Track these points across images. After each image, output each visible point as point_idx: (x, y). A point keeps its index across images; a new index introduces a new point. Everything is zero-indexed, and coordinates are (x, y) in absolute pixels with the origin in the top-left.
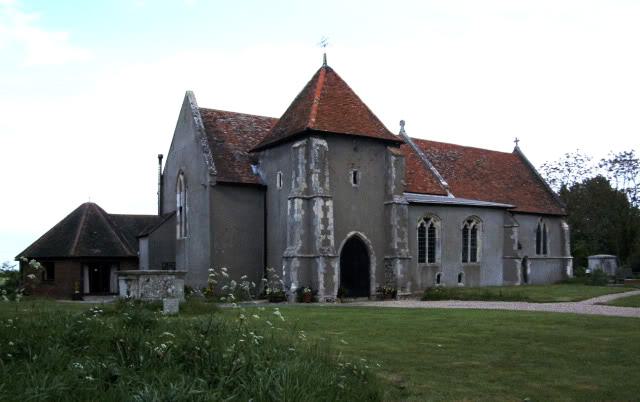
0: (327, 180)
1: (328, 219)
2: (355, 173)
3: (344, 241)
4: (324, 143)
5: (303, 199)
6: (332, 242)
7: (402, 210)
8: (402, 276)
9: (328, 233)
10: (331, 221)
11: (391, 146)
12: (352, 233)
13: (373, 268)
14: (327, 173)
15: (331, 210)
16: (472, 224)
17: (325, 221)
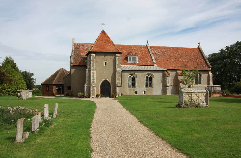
0: (95, 65)
1: (94, 76)
2: (106, 63)
3: (101, 82)
4: (94, 55)
5: (88, 70)
6: (95, 82)
7: (120, 72)
8: (118, 91)
9: (94, 79)
10: (95, 76)
11: (92, 53)
12: (104, 79)
13: (111, 89)
14: (95, 63)
15: (95, 73)
16: (150, 76)
17: (93, 76)
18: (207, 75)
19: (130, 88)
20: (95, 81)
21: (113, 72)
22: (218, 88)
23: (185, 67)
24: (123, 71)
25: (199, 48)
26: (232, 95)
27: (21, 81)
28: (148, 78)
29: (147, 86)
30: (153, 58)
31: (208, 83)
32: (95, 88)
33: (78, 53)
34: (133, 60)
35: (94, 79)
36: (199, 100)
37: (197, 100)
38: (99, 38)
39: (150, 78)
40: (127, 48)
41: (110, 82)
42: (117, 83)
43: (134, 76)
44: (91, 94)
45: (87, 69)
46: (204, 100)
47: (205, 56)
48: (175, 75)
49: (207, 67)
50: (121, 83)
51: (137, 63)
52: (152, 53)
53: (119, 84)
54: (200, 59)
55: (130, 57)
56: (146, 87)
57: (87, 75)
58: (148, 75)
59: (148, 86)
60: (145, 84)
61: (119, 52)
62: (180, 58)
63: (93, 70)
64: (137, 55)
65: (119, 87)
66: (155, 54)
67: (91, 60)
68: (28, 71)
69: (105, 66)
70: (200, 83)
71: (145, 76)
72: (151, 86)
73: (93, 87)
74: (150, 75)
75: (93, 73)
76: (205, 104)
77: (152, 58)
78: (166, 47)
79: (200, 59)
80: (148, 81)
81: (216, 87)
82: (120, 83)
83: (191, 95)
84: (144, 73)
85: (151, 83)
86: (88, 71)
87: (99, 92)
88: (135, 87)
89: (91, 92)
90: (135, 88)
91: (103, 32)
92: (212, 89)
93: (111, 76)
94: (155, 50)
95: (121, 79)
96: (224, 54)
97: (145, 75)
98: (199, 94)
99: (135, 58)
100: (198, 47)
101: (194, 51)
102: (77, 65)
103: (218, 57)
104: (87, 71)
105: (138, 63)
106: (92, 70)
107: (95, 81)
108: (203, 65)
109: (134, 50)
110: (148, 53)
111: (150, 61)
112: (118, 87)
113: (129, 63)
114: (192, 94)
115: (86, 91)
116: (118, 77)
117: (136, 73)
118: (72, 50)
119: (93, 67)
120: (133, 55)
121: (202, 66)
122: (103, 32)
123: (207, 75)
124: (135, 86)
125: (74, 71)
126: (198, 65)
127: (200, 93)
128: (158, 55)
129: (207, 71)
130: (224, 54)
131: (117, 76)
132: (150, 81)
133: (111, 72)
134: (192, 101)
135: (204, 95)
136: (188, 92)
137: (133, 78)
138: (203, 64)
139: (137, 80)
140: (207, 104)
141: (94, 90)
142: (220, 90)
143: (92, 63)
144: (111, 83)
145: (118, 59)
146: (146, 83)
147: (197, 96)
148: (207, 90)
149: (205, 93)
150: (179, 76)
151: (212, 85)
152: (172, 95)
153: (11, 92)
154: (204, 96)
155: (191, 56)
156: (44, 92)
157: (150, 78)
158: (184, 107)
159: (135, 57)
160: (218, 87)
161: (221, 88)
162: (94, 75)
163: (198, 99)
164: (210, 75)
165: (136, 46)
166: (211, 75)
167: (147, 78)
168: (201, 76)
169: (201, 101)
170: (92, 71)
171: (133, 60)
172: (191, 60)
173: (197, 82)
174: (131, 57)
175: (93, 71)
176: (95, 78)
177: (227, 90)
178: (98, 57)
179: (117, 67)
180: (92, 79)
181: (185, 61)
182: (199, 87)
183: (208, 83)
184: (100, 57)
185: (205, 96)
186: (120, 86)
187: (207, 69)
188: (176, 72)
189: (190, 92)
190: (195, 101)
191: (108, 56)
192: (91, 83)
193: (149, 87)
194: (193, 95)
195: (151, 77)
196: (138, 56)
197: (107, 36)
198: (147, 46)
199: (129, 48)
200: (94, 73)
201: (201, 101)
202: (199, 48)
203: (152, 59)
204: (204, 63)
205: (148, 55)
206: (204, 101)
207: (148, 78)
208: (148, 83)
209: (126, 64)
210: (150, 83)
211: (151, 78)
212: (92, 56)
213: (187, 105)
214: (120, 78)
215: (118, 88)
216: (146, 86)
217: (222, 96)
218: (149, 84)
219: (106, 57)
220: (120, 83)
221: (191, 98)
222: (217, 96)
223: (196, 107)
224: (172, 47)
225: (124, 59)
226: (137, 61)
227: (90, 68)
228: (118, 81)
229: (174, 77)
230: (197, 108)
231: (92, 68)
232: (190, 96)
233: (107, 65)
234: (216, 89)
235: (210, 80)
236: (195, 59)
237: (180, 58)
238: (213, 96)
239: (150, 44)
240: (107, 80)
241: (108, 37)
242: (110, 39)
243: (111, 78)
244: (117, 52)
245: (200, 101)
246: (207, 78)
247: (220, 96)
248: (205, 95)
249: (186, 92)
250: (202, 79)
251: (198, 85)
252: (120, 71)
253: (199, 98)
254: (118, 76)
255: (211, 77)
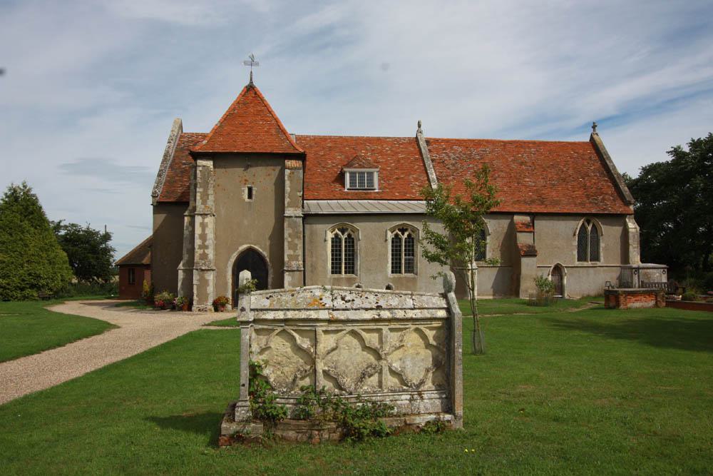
0: (211, 198)
2: (250, 190)
4: (210, 164)
9: (207, 247)
11: (201, 159)
12: (245, 246)
14: (211, 191)
16: (406, 234)
17: (203, 237)
18: (622, 228)
19: (336, 276)
20: (211, 253)
21: (276, 219)
22: (655, 274)
23: (543, 203)
24: (307, 218)
25: (594, 144)
26: (704, 302)
27: (44, 255)
28: (340, 242)
29: (396, 268)
30: (433, 176)
31: (625, 257)
32: (210, 277)
33: (184, 164)
34: (362, 183)
35: (207, 247)
36: (381, 373)
37: (363, 377)
38: (234, 109)
39: (409, 242)
40: (349, 146)
41: (265, 254)
42: (286, 259)
43: (349, 235)
44: (195, 297)
45: (186, 213)
46: (427, 371)
47: (618, 174)
48: (505, 231)
49: (619, 203)
50: (301, 258)
51: (377, 191)
52: (433, 160)
53: (294, 263)
54: (595, 178)
55: (350, 173)
56: (392, 272)
57: (186, 232)
58: (400, 230)
59: (400, 267)
60: (388, 262)
61: (297, 152)
62: (527, 174)
63: (204, 215)
64: (376, 167)
65: (291, 273)
66: (439, 163)
67: (199, 180)
68: (94, 227)
69: (247, 200)
70: (596, 257)
71: (390, 236)
72: (413, 267)
73: (201, 273)
74: (406, 230)
75: (203, 226)
76: (428, 406)
77: (428, 176)
78: (480, 141)
79: (596, 176)
80: (400, 250)
81: (648, 271)
82: (297, 260)
83: (315, 342)
84: (383, 223)
85: (411, 257)
86: (189, 218)
87: (226, 289)
88: (353, 273)
89: (195, 291)
90: (354, 276)
91: (251, 88)
92: (636, 278)
93: (267, 236)
94: (444, 149)
95: (300, 245)
96: (682, 164)
97: (390, 230)
98: (379, 331)
99: (371, 174)
100: (592, 138)
101: (575, 153)
102: (172, 200)
103: (665, 174)
104: (186, 219)
105: (377, 193)
106: (198, 214)
107: (211, 253)
108: (607, 197)
109: (373, 150)
110: (416, 159)
111: (419, 186)
112: (287, 271)
113: (348, 194)
114: (319, 330)
115: (182, 289)
116: (290, 240)
117: (357, 225)
118: (166, 156)
119: (203, 206)
120: (364, 167)
121: (603, 199)
122: (251, 88)
123: (617, 230)
124: (355, 269)
125: (162, 220)
126: (588, 197)
127: (389, 320)
128: (453, 165)
129: (619, 218)
130: (682, 164)
131: (286, 235)
132: (409, 250)
133: (271, 221)
134: (323, 383)
135: (424, 337)
136: (290, 315)
137: (346, 242)
138: (606, 194)
139: (361, 246)
140: (449, 407)
141: (204, 283)
142: (664, 279)
143: (201, 190)
144: (268, 260)
145: (289, 177)
146: (392, 259)
147: (366, 348)
148: (452, 295)
149: (436, 324)
150: (518, 234)
151: (642, 265)
152: (497, 297)
153: (8, 289)
154: (428, 346)
155: (564, 166)
156: (123, 288)
157: (409, 242)
158: (237, 438)
159: (367, 173)
160: (655, 271)
161: (668, 275)
162: (206, 232)
163: (370, 366)
164: (630, 230)
165: (379, 140)
166: (634, 230)
167: (397, 242)
168: (600, 234)
169: (403, 382)
170: (198, 219)
171: (362, 183)
172: (564, 180)
173: (586, 253)
174: (364, 173)
175: (204, 218)
176: (211, 242)
177: (690, 280)
178: (223, 170)
179: (286, 203)
180: (200, 247)
181: (542, 182)
182: (591, 270)
183: (625, 257)
184: (230, 170)
185: (432, 341)
186: (295, 269)
187: (618, 208)
188: (509, 221)
189: (303, 315)
190: (348, 382)
191: (260, 168)
192: (197, 258)
193: (405, 272)
194: (326, 342)
195: (413, 239)
196: (378, 170)
197: (262, 100)
198: (417, 138)
199: (357, 144)
200: (207, 226)
201: (403, 382)
202: (594, 141)
203: (429, 180)
204: (612, 190)
205: (416, 167)
206: (422, 382)
207: (400, 239)
208: (400, 259)
209: (338, 196)
210: (409, 260)
211: (413, 242)
212: (201, 169)
213: (268, 418)
214: (296, 241)
215: (289, 275)
216: (392, 267)
217: (664, 304)
218: (403, 261)
219: (252, 170)
220: (297, 260)
221: (313, 363)
222: (646, 305)
223: (343, 437)
224: (503, 142)
225: (333, 179)
226: (376, 186)
227: (195, 208)
228: (291, 252)
229: (501, 238)
230: (347, 450)
231: (200, 207)
232: (305, 343)
233: (254, 198)
234: (649, 278)
235: (631, 247)
236: (578, 178)
237: (527, 174)
238: (629, 305)
239: (429, 133)
240: (256, 247)
241: (266, 106)
242: (270, 112)
243: (268, 243)
244: (291, 151)
245: (391, 381)
246: (619, 241)
247: (656, 305)
248: (430, 334)
249: (270, 316)
250: (602, 245)
251: (589, 263)
252: (296, 217)
253: (379, 358)
254: (290, 235)
255: (634, 238)
